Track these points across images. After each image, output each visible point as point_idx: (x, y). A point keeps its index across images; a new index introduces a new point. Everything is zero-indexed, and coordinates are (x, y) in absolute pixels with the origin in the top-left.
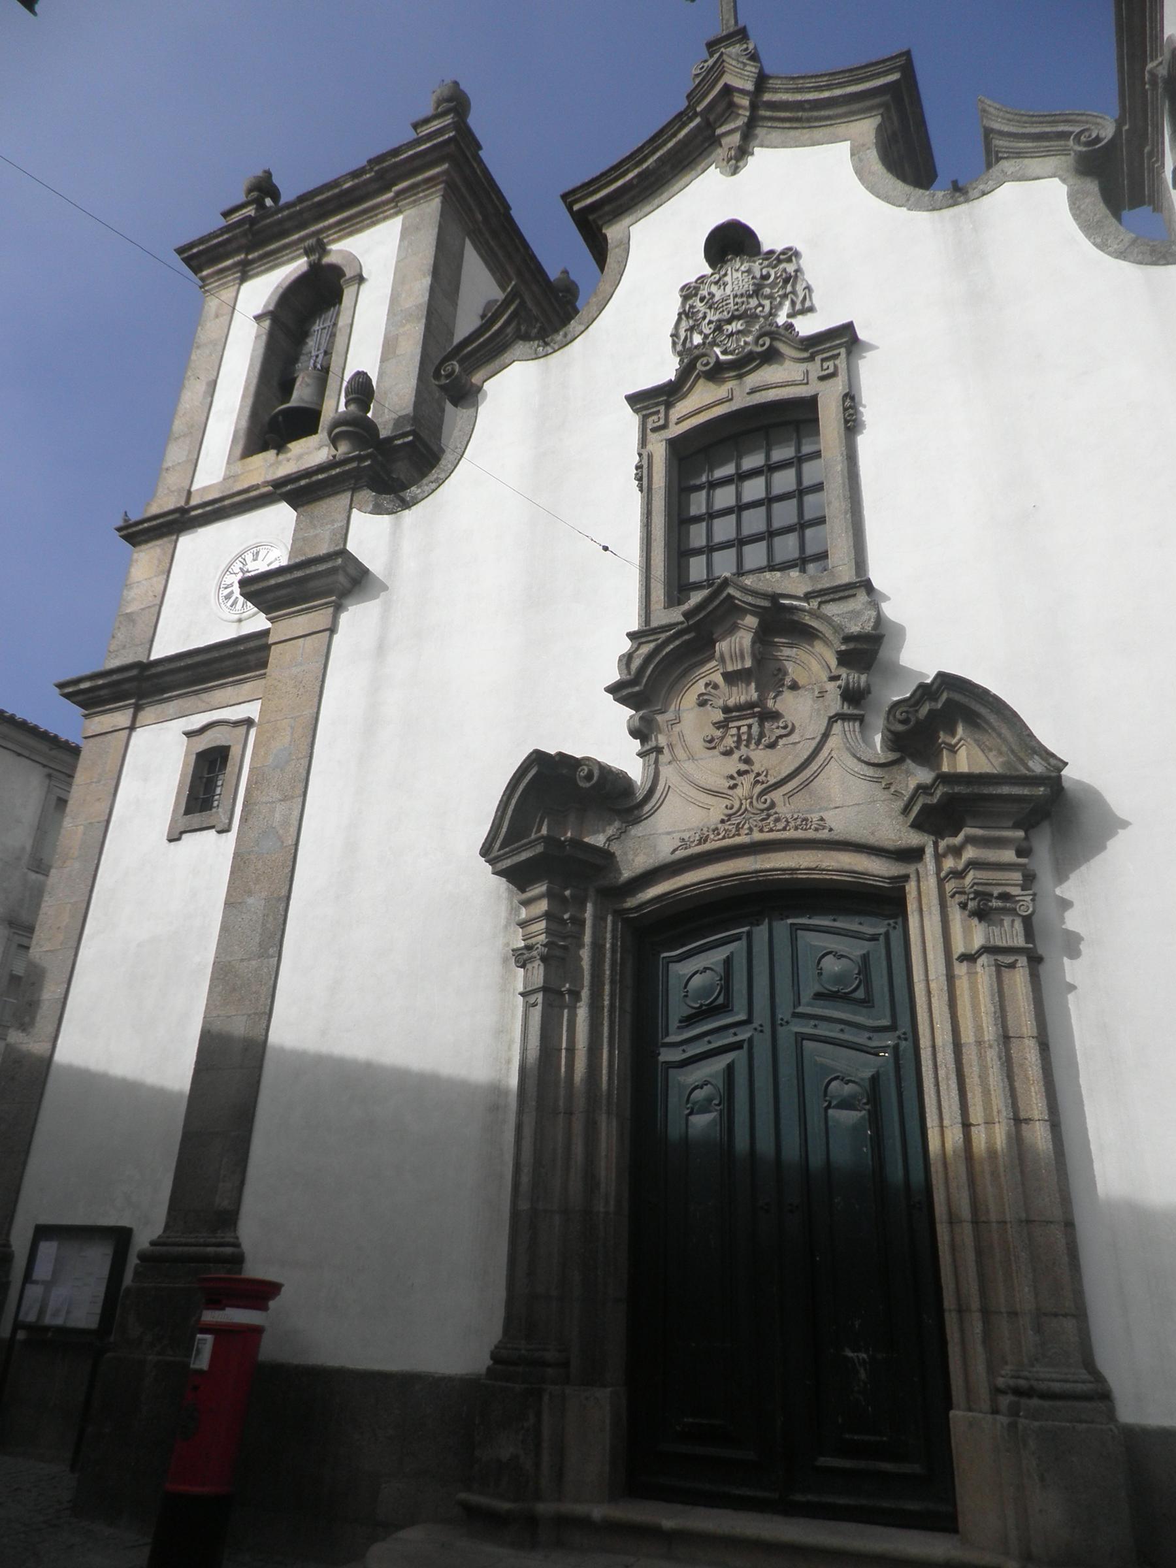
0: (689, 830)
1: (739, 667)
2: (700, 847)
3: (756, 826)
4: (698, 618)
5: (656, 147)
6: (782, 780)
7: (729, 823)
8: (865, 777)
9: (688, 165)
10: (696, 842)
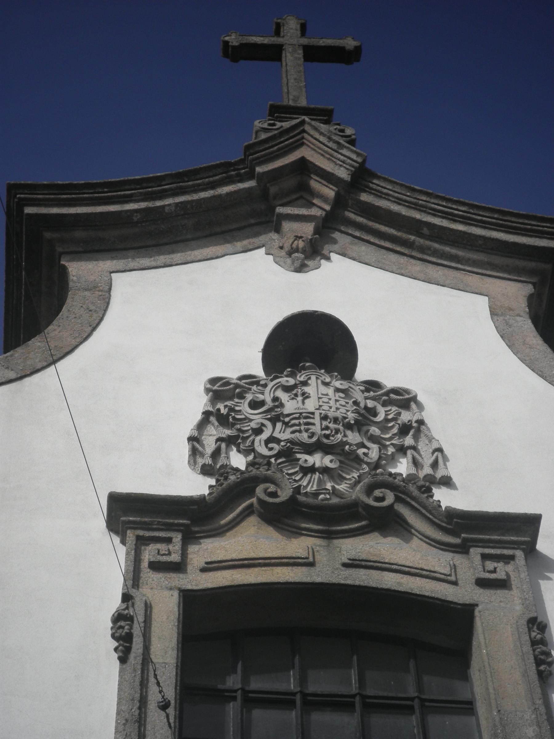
5: (181, 188)
9: (223, 232)
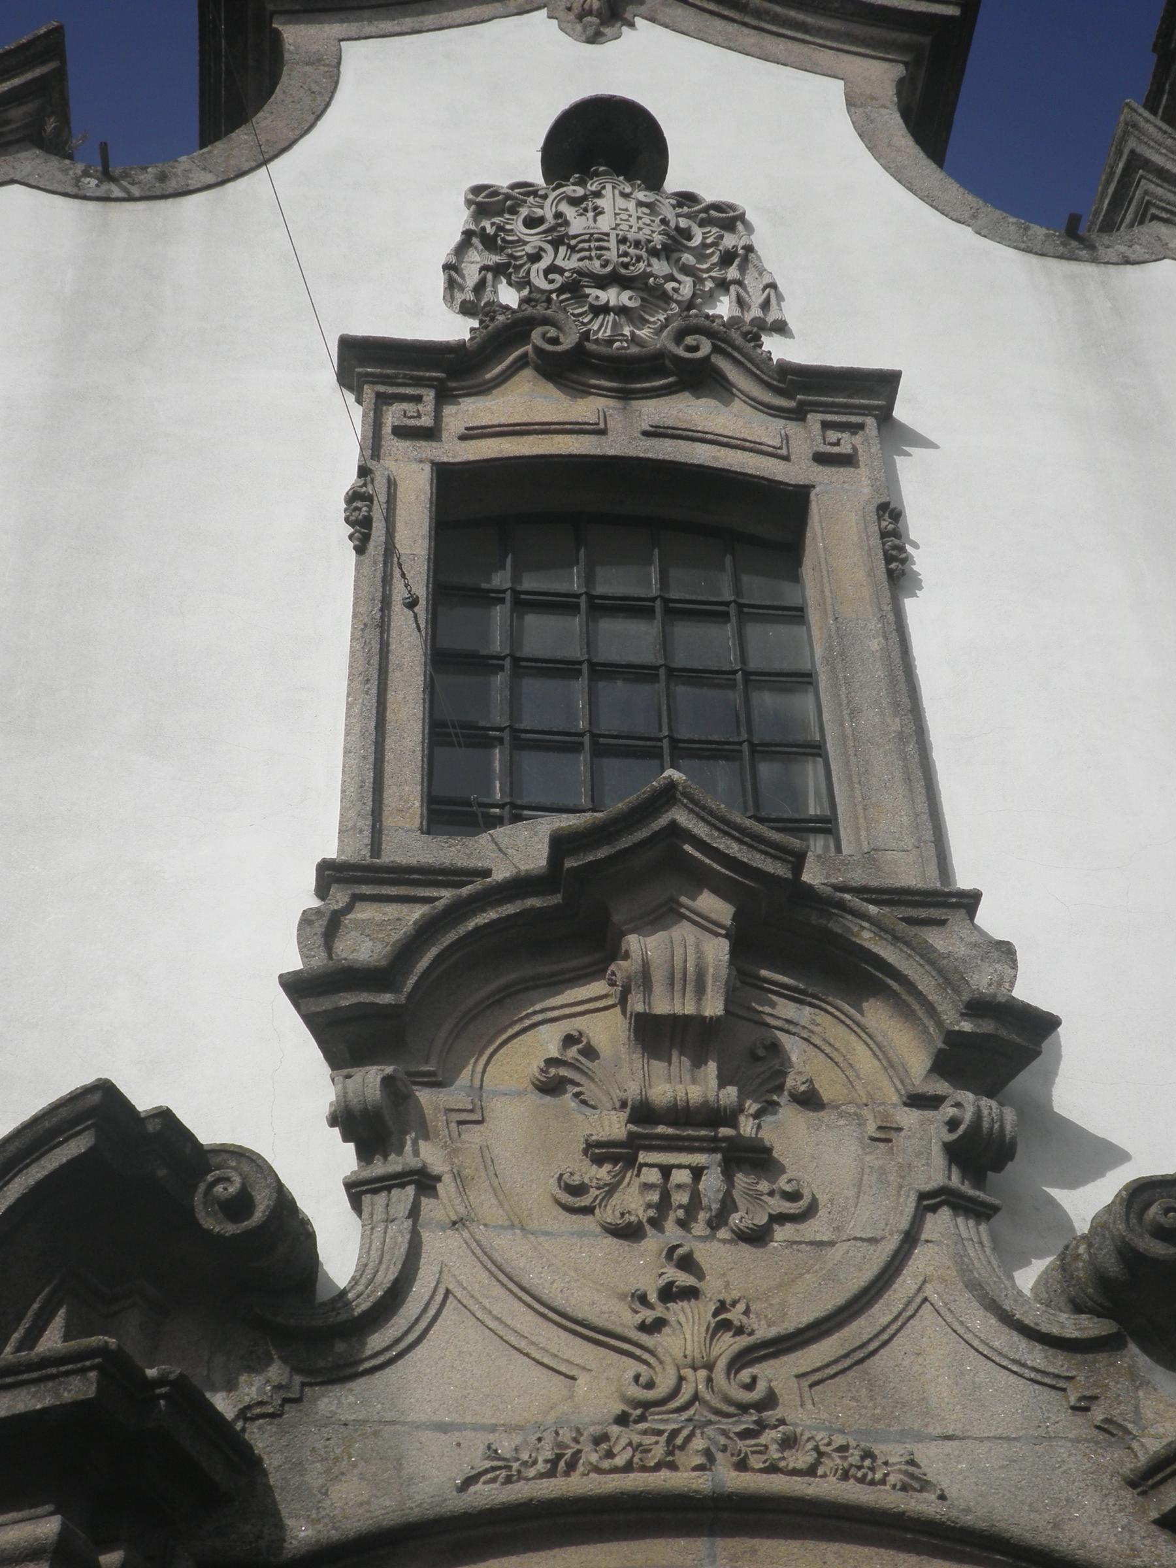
0: (509, 1429)
1: (690, 1009)
2: (545, 1482)
3: (724, 1449)
4: (591, 858)
6: (799, 1332)
7: (642, 1426)
8: (1016, 1368)
10: (541, 1467)
